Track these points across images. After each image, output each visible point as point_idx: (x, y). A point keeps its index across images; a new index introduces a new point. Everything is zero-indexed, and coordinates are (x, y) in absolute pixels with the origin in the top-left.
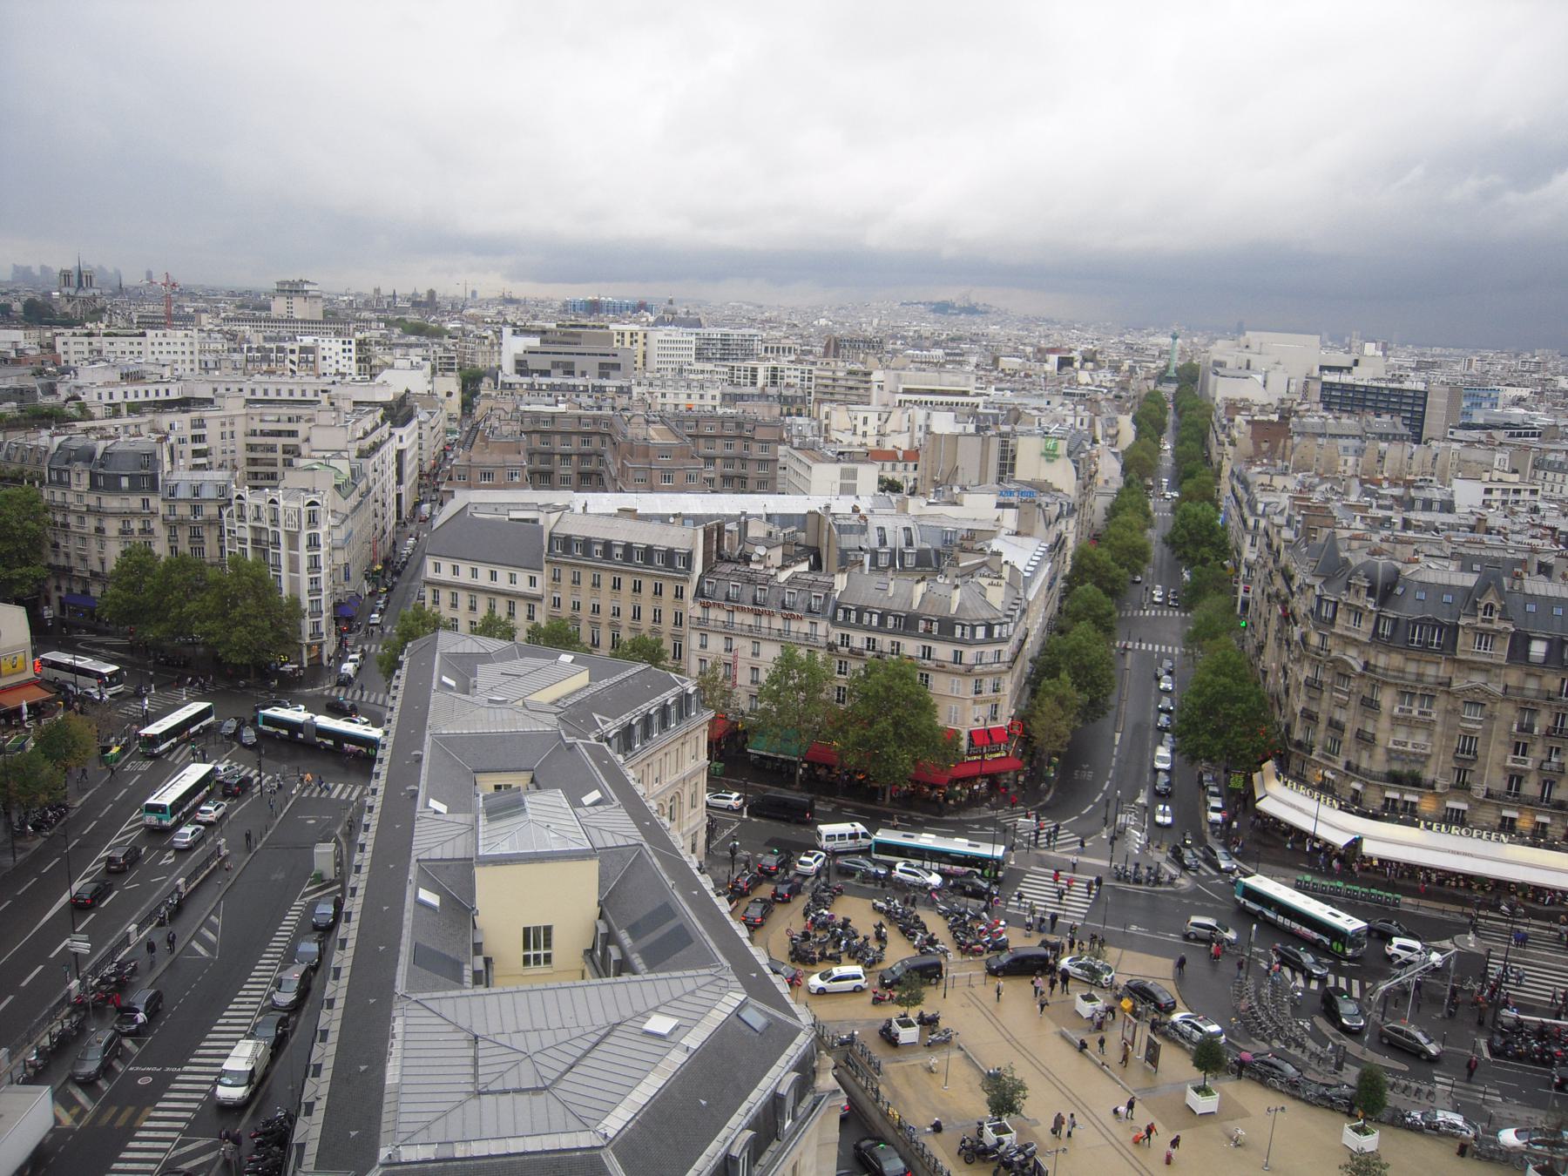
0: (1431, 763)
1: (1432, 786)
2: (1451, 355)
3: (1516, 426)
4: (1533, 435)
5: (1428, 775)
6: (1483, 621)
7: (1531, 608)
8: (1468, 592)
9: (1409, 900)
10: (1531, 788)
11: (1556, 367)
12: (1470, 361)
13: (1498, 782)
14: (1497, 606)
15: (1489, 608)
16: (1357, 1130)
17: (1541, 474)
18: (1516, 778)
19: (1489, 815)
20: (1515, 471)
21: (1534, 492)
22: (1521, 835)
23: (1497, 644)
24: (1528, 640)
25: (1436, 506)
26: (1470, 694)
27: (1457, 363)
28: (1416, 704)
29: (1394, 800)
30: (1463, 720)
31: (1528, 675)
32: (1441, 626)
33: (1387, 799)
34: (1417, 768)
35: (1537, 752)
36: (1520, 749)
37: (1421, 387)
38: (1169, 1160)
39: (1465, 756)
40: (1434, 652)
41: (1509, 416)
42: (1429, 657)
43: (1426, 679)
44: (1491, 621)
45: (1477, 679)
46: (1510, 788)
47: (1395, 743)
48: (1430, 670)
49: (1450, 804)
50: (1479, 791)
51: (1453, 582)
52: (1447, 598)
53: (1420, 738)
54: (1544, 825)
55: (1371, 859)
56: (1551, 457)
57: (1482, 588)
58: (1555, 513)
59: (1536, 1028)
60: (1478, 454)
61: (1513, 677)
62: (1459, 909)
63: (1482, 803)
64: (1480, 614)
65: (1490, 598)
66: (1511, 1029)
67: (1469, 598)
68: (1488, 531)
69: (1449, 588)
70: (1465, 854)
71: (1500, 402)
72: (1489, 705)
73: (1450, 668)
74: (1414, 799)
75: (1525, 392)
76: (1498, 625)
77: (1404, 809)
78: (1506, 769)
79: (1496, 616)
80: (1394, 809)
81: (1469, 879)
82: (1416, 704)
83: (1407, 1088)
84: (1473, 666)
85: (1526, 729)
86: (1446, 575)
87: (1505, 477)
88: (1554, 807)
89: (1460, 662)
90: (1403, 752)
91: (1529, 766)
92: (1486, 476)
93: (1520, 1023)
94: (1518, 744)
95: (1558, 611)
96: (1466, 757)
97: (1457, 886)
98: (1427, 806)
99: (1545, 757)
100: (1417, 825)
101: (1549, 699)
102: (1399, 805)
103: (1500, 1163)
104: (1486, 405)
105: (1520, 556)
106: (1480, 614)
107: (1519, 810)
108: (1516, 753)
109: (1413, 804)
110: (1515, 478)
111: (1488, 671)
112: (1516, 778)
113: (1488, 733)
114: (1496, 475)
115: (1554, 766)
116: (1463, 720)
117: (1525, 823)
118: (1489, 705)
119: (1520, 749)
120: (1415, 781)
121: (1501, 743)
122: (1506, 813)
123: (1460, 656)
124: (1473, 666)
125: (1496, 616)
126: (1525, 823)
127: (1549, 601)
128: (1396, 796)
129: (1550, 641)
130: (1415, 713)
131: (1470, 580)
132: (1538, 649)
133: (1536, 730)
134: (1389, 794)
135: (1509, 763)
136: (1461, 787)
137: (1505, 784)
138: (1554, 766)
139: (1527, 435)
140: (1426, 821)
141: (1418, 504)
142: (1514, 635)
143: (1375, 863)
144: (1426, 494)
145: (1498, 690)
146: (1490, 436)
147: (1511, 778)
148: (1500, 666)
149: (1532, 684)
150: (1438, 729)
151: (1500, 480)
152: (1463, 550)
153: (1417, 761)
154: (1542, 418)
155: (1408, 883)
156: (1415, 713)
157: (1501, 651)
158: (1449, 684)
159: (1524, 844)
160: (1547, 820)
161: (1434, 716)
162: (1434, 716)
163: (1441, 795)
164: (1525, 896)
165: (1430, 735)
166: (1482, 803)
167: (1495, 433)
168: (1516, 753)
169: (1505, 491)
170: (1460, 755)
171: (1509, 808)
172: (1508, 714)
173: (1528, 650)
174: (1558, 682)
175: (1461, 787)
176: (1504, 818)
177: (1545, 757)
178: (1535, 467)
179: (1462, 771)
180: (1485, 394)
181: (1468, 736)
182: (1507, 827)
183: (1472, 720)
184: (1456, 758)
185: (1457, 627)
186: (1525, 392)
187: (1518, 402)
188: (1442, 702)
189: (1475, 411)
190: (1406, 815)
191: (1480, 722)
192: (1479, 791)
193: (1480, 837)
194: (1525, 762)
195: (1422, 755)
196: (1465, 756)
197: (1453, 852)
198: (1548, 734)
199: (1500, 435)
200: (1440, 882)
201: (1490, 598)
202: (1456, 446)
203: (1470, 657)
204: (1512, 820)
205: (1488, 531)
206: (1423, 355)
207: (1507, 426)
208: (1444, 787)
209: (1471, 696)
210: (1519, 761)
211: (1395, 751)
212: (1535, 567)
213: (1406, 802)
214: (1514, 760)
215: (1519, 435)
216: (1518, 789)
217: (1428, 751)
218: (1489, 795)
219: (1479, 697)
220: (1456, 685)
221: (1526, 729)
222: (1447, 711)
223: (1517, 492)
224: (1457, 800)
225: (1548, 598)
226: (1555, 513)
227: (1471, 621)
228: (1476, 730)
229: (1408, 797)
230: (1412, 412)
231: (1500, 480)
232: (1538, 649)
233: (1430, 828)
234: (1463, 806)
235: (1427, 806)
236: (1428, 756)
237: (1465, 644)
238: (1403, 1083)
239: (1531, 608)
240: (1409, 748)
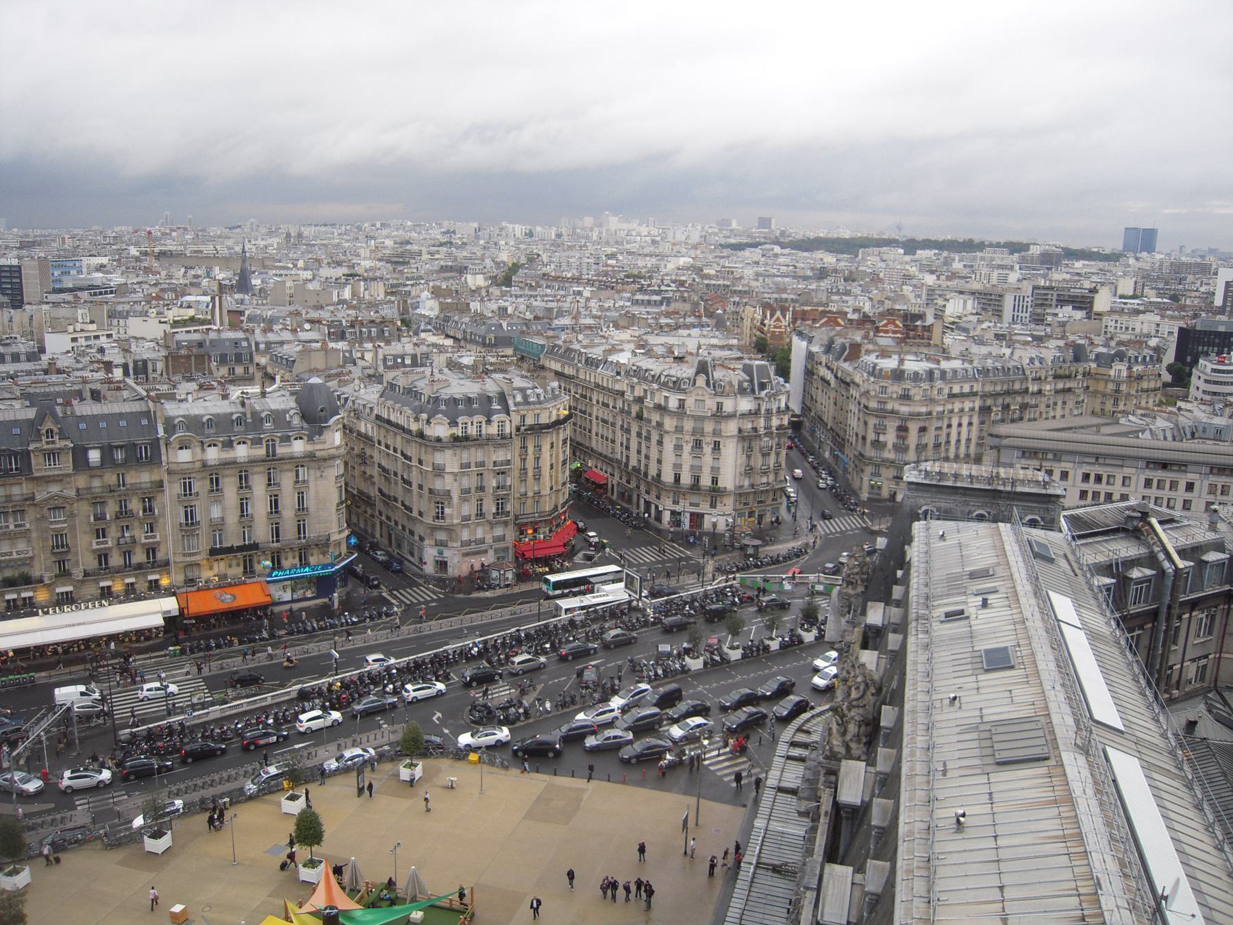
0: (36, 563)
1: (41, 581)
2: (50, 235)
3: (98, 287)
4: (111, 292)
5: (36, 572)
6: (48, 443)
7: (83, 426)
8: (31, 423)
9: (43, 674)
10: (116, 560)
11: (130, 240)
12: (63, 239)
13: (91, 563)
14: (56, 430)
15: (50, 432)
16: (10, 874)
17: (115, 322)
18: (103, 557)
19: (91, 589)
20: (92, 322)
21: (109, 336)
22: (118, 596)
23: (63, 458)
24: (85, 451)
25: (23, 357)
26: (51, 502)
27: (54, 241)
28: (11, 520)
29: (14, 600)
30: (51, 523)
31: (92, 477)
32: (15, 454)
33: (8, 601)
34: (25, 569)
35: (113, 532)
36: (101, 533)
37: (15, 262)
38: (428, 810)
39: (61, 550)
40: (14, 476)
41: (91, 280)
42: (12, 480)
43: (14, 498)
44: (53, 442)
45: (54, 489)
46: (100, 564)
47: (18, 553)
48: (16, 491)
49: (59, 590)
50: (78, 574)
51: (19, 417)
52: (16, 431)
53: (22, 545)
54: (132, 584)
55: (6, 652)
56: (120, 308)
57: (41, 418)
58: (116, 350)
59: (145, 733)
60: (63, 312)
61: (81, 481)
62: (82, 667)
63: (83, 582)
64: (44, 438)
65: (49, 425)
66: (129, 742)
67: (32, 428)
68: (59, 372)
69: (15, 423)
70: (79, 624)
71: (85, 270)
72: (68, 507)
73: (30, 486)
74: (30, 594)
75: (104, 260)
76: (60, 444)
77: (24, 605)
78: (94, 551)
79: (56, 438)
80: (16, 607)
81: (87, 642)
82: (11, 520)
83: (53, 820)
84: (48, 480)
85: (100, 518)
86: (12, 413)
87: (85, 327)
88: (136, 569)
89: (37, 478)
90: (10, 561)
91: (110, 544)
92: (71, 329)
93: (133, 735)
94: (98, 531)
95: (103, 425)
96: (61, 551)
97: (79, 650)
98: (42, 596)
99: (119, 534)
100: (36, 614)
101: (111, 491)
102: (20, 603)
103: (126, 844)
104: (73, 272)
105: (76, 387)
106: (44, 438)
107: (159, 573)
108: (98, 537)
109: (30, 598)
110: (93, 327)
111: (61, 481)
112: (103, 557)
113: (72, 528)
114: (79, 327)
115: (128, 540)
116: (51, 523)
117: (118, 587)
118: (68, 507)
119: (101, 533)
120: (27, 581)
121: (85, 533)
122: (102, 584)
123: (36, 474)
124: (48, 480)
125: (56, 438)
126: (118, 587)
127: (95, 419)
128: (15, 596)
129: (101, 448)
130: (12, 527)
131: (31, 414)
132: (94, 456)
133: (108, 517)
134: (8, 597)
135: (95, 547)
136: (64, 574)
137: (96, 562)
138: (128, 540)
139: (106, 293)
140: (42, 609)
141: (8, 358)
142: (74, 449)
143: (11, 654)
144: (14, 349)
145: (73, 493)
146: (76, 296)
147: (100, 557)
148: (69, 475)
149: (96, 483)
150: (34, 535)
151: (82, 330)
152: (31, 390)
153: (24, 564)
154: (116, 279)
155: (40, 661)
156: (12, 527)
157: (66, 464)
158: (33, 498)
159: (121, 602)
160: (132, 580)
161: (28, 526)
162: (28, 526)
163: (49, 585)
164: (130, 640)
165: (29, 541)
166: (83, 582)
167: (79, 294)
168: (98, 537)
169: (87, 338)
170: (56, 550)
171: (104, 579)
172: (84, 510)
173: (87, 459)
174: (115, 477)
175: (64, 574)
176: (103, 588)
177: (119, 534)
178: (109, 317)
179: (61, 563)
180: (71, 264)
181: (59, 535)
182: (107, 595)
183: (58, 522)
184: (53, 553)
185: (28, 452)
186: (104, 260)
187: (101, 268)
188: (31, 514)
189: (64, 278)
190: (26, 609)
191: (65, 522)
192: (78, 574)
193: (87, 608)
194: (106, 543)
195: (26, 559)
196: (61, 550)
197: (70, 626)
198: (117, 518)
199: (84, 295)
200: (66, 652)
201: (49, 425)
202: (45, 307)
203: (44, 474)
204: (109, 587)
205: (59, 372)
206: (27, 236)
207: (91, 287)
208: (51, 578)
209: (52, 503)
210: (102, 543)
211: (20, 559)
212: (89, 394)
213: (24, 599)
214: (98, 543)
215: (101, 293)
216: (154, 557)
217: (31, 554)
218: (86, 574)
219: (58, 502)
220: (38, 497)
221: (100, 518)
222: (37, 519)
223: (97, 337)
224: (64, 585)
225: (94, 416)
226: (116, 350)
227: (38, 445)
228: (63, 529)
229: (24, 595)
230: (11, 283)
231: (82, 330)
232: (94, 456)
233: (47, 613)
234: (70, 588)
235: (42, 596)
236: (32, 558)
237: (38, 464)
238: (49, 818)
239: (83, 426)
240: (15, 556)
